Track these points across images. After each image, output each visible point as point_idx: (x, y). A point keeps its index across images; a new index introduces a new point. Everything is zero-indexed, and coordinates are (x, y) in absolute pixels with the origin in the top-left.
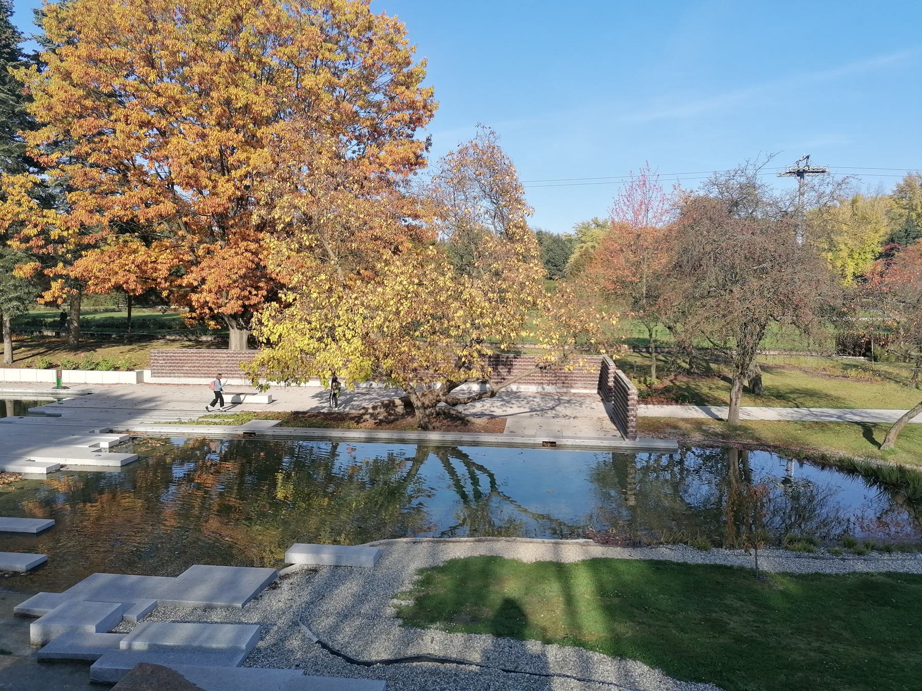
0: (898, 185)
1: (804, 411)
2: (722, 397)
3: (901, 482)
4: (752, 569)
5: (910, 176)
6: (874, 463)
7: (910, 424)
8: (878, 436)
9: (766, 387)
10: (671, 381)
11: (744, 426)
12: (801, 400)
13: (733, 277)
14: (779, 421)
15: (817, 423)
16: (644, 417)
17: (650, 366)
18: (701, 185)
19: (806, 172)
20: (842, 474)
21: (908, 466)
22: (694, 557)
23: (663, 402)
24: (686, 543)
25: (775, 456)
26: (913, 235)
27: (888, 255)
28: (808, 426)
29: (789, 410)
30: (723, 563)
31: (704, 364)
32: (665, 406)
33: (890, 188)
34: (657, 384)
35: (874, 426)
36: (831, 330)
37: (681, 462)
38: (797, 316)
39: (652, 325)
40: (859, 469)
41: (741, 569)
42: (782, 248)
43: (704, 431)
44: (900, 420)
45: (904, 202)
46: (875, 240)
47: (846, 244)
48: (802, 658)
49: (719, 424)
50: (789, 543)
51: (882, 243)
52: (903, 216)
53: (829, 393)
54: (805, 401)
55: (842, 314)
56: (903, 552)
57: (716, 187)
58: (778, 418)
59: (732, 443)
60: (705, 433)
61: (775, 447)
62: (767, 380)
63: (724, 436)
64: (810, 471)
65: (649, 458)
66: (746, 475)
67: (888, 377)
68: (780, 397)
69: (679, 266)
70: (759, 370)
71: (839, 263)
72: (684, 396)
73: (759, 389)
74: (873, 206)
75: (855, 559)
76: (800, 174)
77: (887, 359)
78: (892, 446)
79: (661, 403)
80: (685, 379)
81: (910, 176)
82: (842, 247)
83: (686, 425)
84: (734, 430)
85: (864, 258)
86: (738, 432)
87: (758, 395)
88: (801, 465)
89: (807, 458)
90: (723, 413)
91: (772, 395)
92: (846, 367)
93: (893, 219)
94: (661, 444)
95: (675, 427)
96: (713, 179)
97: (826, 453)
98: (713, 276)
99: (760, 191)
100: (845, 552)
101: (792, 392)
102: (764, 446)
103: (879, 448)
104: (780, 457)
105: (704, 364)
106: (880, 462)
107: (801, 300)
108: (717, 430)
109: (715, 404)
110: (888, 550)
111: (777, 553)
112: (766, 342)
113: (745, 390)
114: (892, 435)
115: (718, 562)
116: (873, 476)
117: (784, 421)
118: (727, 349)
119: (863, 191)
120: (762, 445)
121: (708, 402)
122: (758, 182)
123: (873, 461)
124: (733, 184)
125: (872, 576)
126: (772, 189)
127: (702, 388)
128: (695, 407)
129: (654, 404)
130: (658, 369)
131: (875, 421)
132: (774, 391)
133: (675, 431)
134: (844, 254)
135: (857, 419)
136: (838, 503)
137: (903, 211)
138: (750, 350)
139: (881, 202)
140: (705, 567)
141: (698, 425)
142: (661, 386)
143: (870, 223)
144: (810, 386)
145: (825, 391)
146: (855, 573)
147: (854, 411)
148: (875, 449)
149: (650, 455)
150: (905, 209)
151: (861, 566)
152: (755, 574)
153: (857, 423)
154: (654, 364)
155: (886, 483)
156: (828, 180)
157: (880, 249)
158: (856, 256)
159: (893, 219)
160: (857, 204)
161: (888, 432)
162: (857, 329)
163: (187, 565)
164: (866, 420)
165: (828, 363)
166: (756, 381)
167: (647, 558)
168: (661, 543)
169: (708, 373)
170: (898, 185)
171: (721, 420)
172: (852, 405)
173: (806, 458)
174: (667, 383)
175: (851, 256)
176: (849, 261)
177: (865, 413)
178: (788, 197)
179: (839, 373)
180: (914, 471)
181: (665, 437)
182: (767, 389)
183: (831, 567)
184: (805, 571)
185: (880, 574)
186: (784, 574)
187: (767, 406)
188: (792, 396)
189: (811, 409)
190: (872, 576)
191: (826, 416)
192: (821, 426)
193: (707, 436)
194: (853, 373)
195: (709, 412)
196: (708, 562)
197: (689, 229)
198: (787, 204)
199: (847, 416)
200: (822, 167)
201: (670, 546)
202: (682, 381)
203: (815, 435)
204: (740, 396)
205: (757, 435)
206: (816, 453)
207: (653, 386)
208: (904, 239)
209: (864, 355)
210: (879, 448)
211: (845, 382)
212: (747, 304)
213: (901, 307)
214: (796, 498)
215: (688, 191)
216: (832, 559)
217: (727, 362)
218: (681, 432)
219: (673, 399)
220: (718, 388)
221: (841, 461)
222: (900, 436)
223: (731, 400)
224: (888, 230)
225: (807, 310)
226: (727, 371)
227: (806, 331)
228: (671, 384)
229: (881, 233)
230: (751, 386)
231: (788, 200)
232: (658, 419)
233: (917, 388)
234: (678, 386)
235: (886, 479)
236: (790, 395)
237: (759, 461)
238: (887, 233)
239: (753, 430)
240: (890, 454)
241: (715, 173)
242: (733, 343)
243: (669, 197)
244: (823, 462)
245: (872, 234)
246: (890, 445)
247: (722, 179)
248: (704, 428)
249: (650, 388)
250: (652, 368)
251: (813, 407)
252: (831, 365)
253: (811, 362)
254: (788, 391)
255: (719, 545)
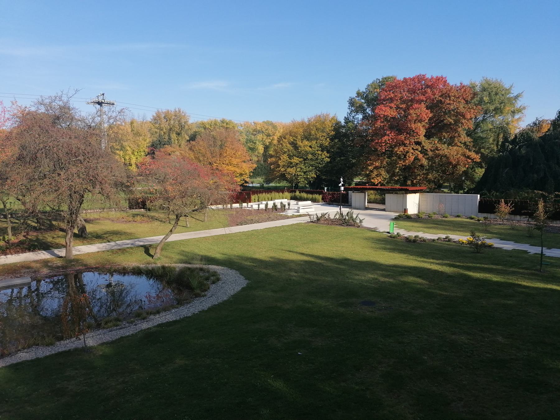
0: (153, 116)
1: (112, 243)
2: (61, 243)
3: (164, 274)
4: (83, 347)
5: (158, 112)
6: (150, 267)
7: (167, 242)
8: (152, 252)
9: (89, 232)
10: (24, 236)
11: (76, 259)
12: (111, 237)
13: (59, 165)
14: (98, 252)
15: (120, 249)
16: (4, 264)
17: (7, 227)
18: (32, 104)
19: (103, 103)
20: (134, 276)
21: (167, 265)
22: (42, 352)
23: (18, 252)
24: (38, 345)
25: (96, 273)
26: (163, 143)
27: (151, 154)
28: (115, 252)
29: (104, 244)
30: (64, 349)
31: (48, 222)
32: (21, 254)
33: (149, 118)
34: (13, 239)
35: (150, 246)
36: (123, 195)
37: (37, 290)
38: (102, 189)
39: (5, 199)
40: (143, 271)
41: (76, 350)
42: (89, 148)
43: (50, 266)
44: (161, 241)
45: (157, 125)
46: (145, 143)
47: (130, 147)
48: (113, 391)
49: (60, 260)
50: (105, 324)
51: (148, 147)
52: (157, 133)
53: (126, 231)
54: (113, 237)
55: (128, 187)
56: (165, 311)
57: (43, 106)
58: (97, 250)
59: (69, 271)
60: (51, 268)
61: (96, 268)
62: (90, 228)
63: (63, 267)
64: (116, 279)
65: (12, 292)
66: (81, 288)
67: (153, 218)
68: (98, 237)
69: (20, 158)
70: (84, 222)
71: (127, 158)
72: (34, 245)
73: (85, 234)
74: (142, 126)
75: (142, 322)
76: (100, 104)
77: (155, 209)
78: (159, 256)
79: (17, 252)
80: (35, 234)
81: (158, 112)
82: (128, 148)
83: (36, 265)
84: (69, 262)
85: (140, 155)
86: (73, 263)
87: (85, 238)
88: (112, 275)
89: (115, 271)
90: (62, 253)
91: (93, 237)
92: (134, 216)
93: (152, 134)
94: (18, 281)
95: (28, 268)
96: (40, 100)
97: (125, 266)
98: (46, 166)
99: (72, 111)
100: (137, 320)
101: (105, 234)
102: (89, 269)
103: (153, 258)
104: (99, 274)
105: (48, 222)
106: (153, 265)
107: (103, 179)
108: (59, 265)
109: (57, 248)
110: (158, 312)
111: (99, 333)
112: (84, 205)
113: (75, 236)
114: (158, 250)
115: (60, 350)
116: (151, 274)
117: (101, 251)
118: (60, 211)
119: (136, 118)
120: (88, 268)
121: (52, 247)
122: (71, 106)
123: (150, 265)
124: (55, 105)
125: (151, 329)
126: (80, 111)
127: (47, 238)
128: (44, 252)
129: (12, 254)
130: (13, 229)
131: (150, 243)
132: (95, 234)
133: (27, 270)
134: (130, 152)
135: (142, 244)
136: (136, 291)
137: (156, 130)
138: (75, 212)
139: (146, 124)
140: (51, 356)
141: (45, 263)
142: (17, 241)
143: (141, 136)
144: (115, 229)
145: (124, 231)
146: (142, 330)
147: (140, 240)
148: (151, 259)
149: (13, 290)
150: (158, 129)
151: (145, 326)
152: (86, 350)
153: (141, 246)
154: (10, 226)
155: (157, 276)
156: (112, 109)
157: (147, 150)
158: (136, 154)
159: (152, 134)
160: (134, 124)
161: (156, 248)
162: (136, 195)
163: (497, 248)
164: (146, 244)
165: (124, 214)
166: (83, 230)
167: (8, 364)
168: (19, 350)
169: (51, 228)
170: (153, 116)
171: (61, 257)
172: (139, 236)
173: (114, 271)
174: (21, 238)
175: (133, 153)
176: (132, 156)
177: (145, 240)
178: (90, 117)
179: (131, 219)
180: (169, 267)
181: (21, 276)
182: (91, 233)
183: (129, 331)
184: (114, 338)
185: (154, 327)
186: (103, 344)
187: (91, 244)
188: (105, 236)
189: (117, 242)
190: (151, 329)
191: (125, 245)
192: (123, 251)
193: (52, 270)
194: (138, 218)
195: (53, 254)
196: (53, 352)
197: (25, 133)
198: (91, 121)
199: (136, 243)
200: (112, 101)
201: (26, 350)
202: (33, 235)
203: (119, 257)
204: (72, 240)
205: (85, 263)
206: (120, 267)
207: (11, 242)
208: (159, 145)
209: (143, 208)
210: (153, 258)
211: (135, 224)
212: (70, 183)
213: (157, 182)
214: (113, 293)
215: (24, 107)
216: (130, 326)
217: (63, 220)
218: (33, 270)
219: (26, 249)
220: (58, 237)
221: (134, 269)
222: (162, 249)
223: (66, 243)
224: (151, 140)
225: (107, 185)
226: (63, 225)
227: (108, 197)
228: (24, 239)
229: (148, 141)
230: (80, 233)
231: (91, 119)
232: (15, 265)
233: (170, 223)
234: (29, 239)
235: (156, 274)
236: (104, 235)
237: (88, 278)
238: (150, 142)
239: (82, 260)
240: (158, 260)
241: (41, 96)
242: (65, 207)
243: (9, 109)
244: (124, 272)
245: (143, 142)
246: (158, 255)
247: (47, 101)
248: (49, 264)
249: (8, 243)
250: (8, 229)
251: (117, 241)
252: (127, 215)
253: (113, 214)
254: (103, 233)
255: (61, 339)
